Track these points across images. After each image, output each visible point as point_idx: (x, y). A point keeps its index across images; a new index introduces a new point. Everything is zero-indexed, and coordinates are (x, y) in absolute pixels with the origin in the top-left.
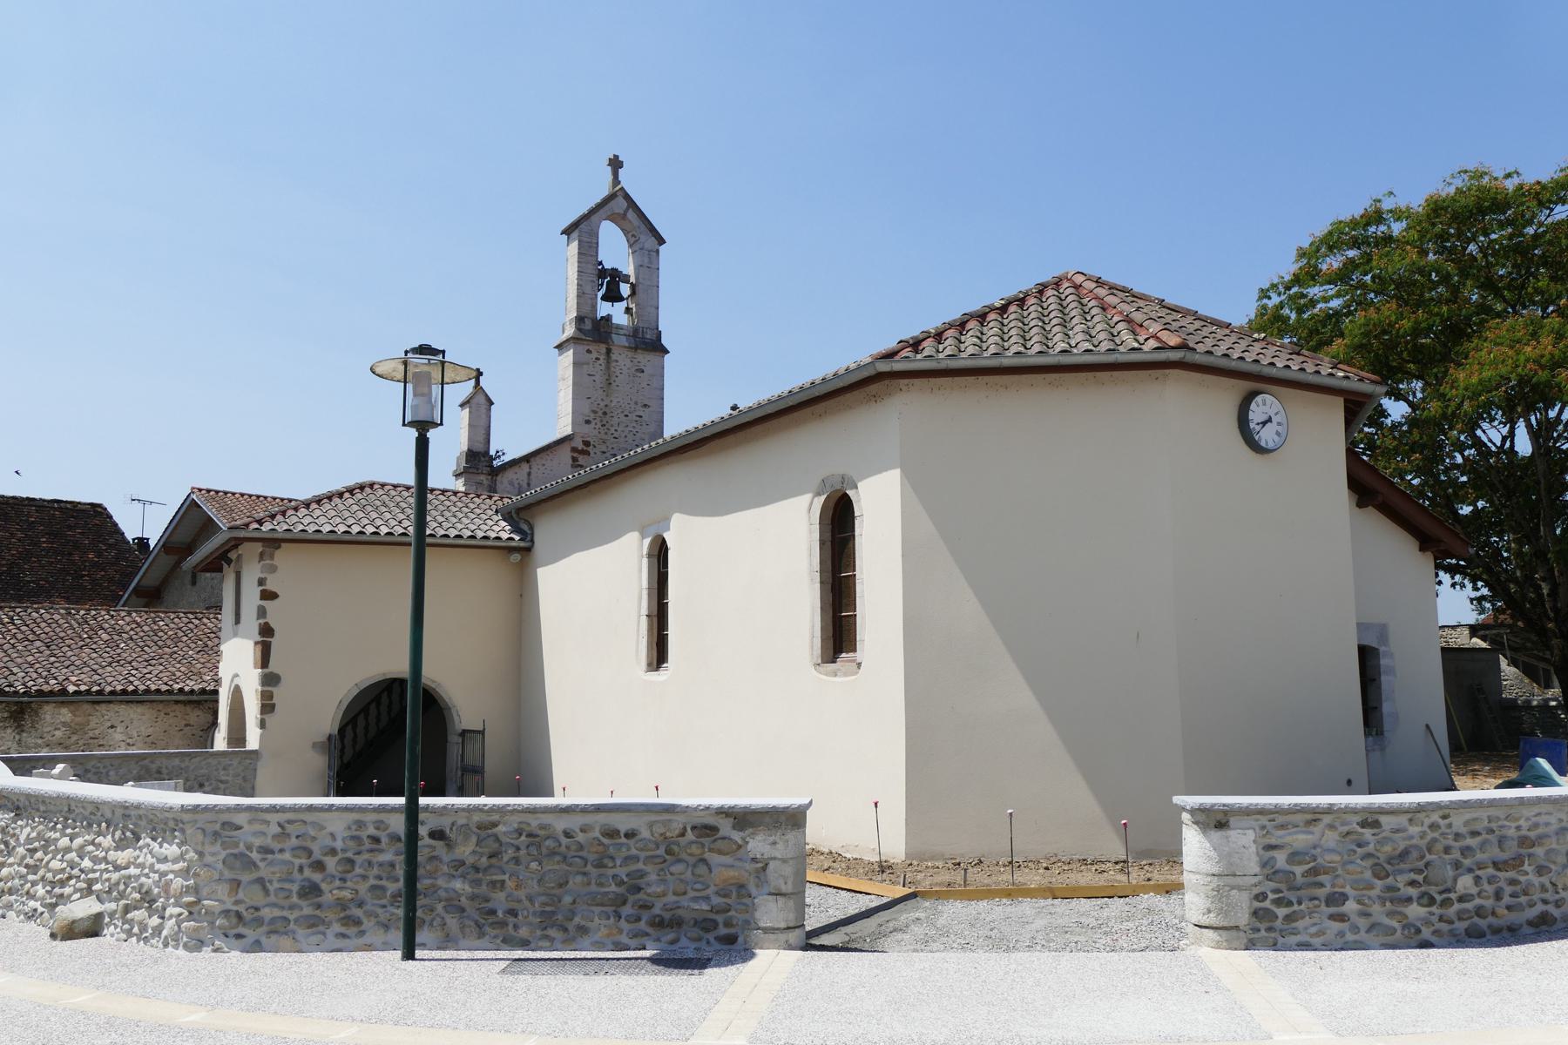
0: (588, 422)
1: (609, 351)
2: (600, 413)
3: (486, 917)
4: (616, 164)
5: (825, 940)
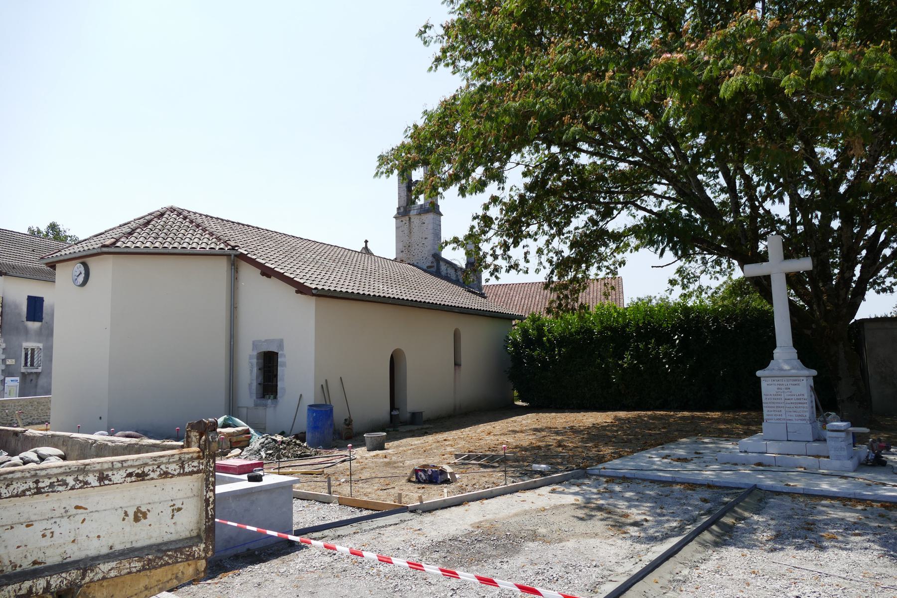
0: (402, 252)
1: (410, 218)
2: (407, 247)
3: (36, 566)
4: (366, 242)
5: (204, 243)
